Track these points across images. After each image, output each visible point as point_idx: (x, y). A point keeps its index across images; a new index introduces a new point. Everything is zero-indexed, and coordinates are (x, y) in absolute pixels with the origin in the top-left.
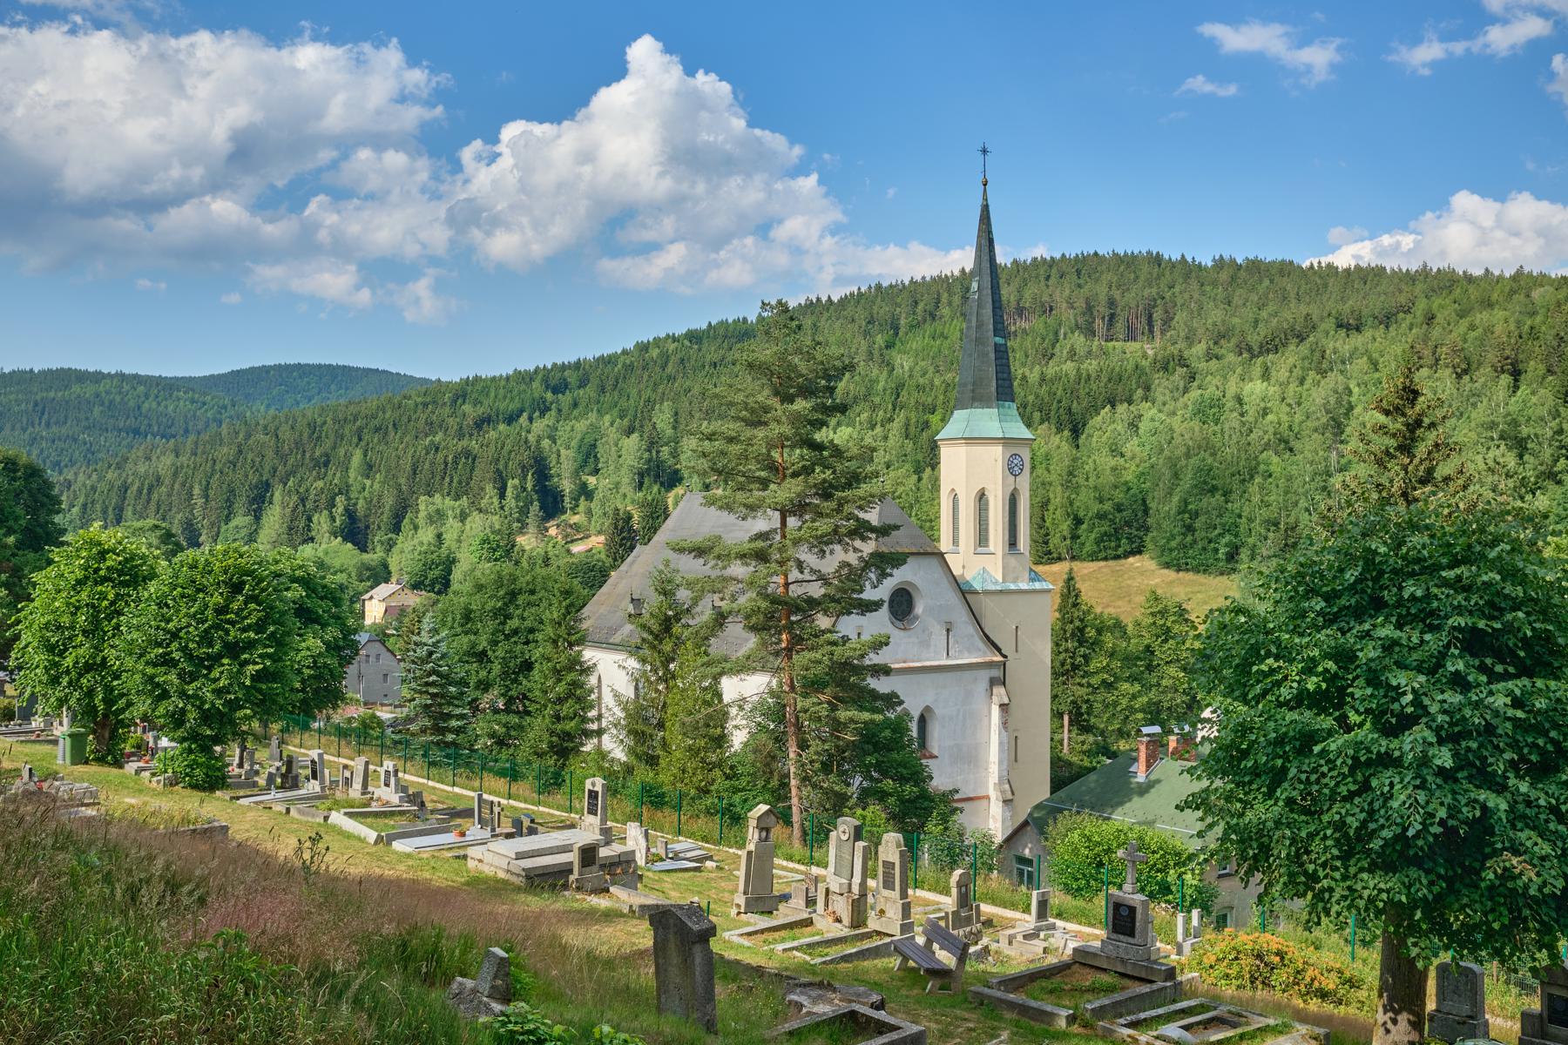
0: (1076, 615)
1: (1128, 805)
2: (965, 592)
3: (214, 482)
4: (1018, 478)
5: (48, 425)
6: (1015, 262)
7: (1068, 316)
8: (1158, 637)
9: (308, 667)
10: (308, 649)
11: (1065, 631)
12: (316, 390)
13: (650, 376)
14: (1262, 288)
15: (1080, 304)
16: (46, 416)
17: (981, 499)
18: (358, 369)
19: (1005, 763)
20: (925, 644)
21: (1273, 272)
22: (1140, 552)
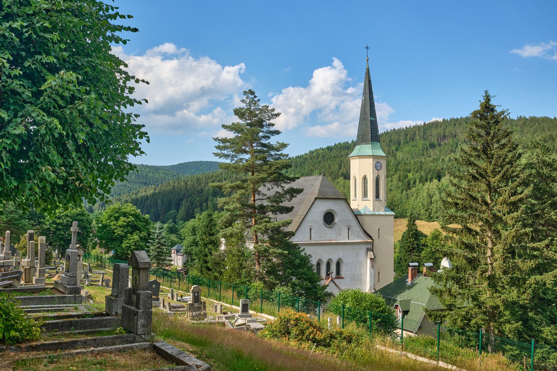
1: (403, 293)
2: (357, 215)
3: (165, 199)
4: (379, 171)
6: (444, 120)
9: (133, 245)
10: (133, 239)
12: (206, 170)
13: (312, 162)
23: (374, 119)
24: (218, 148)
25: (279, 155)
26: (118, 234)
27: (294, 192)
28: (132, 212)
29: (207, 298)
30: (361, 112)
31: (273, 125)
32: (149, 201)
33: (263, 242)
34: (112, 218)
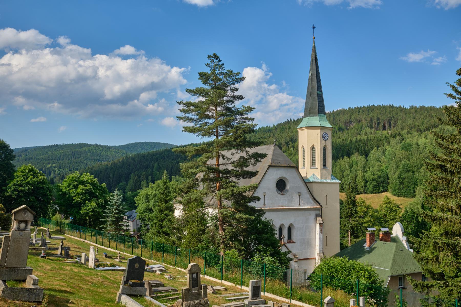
0: (352, 196)
2: (306, 182)
5: (75, 158)
6: (349, 108)
7: (364, 123)
8: (388, 211)
9: (91, 212)
10: (91, 206)
11: (348, 202)
12: (150, 149)
14: (424, 114)
15: (369, 120)
16: (75, 156)
17: (312, 149)
18: (162, 143)
19: (322, 246)
20: (291, 201)
21: (428, 109)
22: (386, 191)
23: (320, 93)
24: (182, 111)
25: (245, 119)
26: (77, 201)
27: (258, 157)
28: (91, 181)
29: (174, 266)
30: (308, 86)
31: (237, 90)
32: (102, 175)
33: (226, 207)
34: (71, 186)
